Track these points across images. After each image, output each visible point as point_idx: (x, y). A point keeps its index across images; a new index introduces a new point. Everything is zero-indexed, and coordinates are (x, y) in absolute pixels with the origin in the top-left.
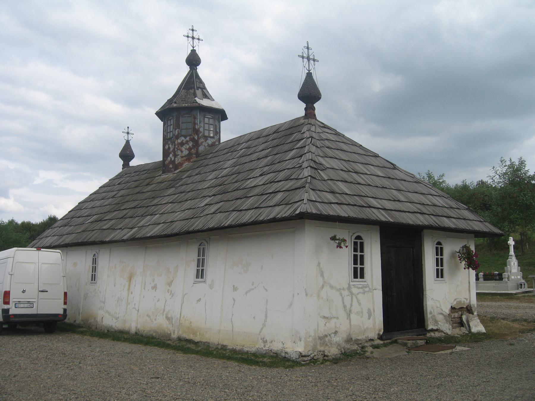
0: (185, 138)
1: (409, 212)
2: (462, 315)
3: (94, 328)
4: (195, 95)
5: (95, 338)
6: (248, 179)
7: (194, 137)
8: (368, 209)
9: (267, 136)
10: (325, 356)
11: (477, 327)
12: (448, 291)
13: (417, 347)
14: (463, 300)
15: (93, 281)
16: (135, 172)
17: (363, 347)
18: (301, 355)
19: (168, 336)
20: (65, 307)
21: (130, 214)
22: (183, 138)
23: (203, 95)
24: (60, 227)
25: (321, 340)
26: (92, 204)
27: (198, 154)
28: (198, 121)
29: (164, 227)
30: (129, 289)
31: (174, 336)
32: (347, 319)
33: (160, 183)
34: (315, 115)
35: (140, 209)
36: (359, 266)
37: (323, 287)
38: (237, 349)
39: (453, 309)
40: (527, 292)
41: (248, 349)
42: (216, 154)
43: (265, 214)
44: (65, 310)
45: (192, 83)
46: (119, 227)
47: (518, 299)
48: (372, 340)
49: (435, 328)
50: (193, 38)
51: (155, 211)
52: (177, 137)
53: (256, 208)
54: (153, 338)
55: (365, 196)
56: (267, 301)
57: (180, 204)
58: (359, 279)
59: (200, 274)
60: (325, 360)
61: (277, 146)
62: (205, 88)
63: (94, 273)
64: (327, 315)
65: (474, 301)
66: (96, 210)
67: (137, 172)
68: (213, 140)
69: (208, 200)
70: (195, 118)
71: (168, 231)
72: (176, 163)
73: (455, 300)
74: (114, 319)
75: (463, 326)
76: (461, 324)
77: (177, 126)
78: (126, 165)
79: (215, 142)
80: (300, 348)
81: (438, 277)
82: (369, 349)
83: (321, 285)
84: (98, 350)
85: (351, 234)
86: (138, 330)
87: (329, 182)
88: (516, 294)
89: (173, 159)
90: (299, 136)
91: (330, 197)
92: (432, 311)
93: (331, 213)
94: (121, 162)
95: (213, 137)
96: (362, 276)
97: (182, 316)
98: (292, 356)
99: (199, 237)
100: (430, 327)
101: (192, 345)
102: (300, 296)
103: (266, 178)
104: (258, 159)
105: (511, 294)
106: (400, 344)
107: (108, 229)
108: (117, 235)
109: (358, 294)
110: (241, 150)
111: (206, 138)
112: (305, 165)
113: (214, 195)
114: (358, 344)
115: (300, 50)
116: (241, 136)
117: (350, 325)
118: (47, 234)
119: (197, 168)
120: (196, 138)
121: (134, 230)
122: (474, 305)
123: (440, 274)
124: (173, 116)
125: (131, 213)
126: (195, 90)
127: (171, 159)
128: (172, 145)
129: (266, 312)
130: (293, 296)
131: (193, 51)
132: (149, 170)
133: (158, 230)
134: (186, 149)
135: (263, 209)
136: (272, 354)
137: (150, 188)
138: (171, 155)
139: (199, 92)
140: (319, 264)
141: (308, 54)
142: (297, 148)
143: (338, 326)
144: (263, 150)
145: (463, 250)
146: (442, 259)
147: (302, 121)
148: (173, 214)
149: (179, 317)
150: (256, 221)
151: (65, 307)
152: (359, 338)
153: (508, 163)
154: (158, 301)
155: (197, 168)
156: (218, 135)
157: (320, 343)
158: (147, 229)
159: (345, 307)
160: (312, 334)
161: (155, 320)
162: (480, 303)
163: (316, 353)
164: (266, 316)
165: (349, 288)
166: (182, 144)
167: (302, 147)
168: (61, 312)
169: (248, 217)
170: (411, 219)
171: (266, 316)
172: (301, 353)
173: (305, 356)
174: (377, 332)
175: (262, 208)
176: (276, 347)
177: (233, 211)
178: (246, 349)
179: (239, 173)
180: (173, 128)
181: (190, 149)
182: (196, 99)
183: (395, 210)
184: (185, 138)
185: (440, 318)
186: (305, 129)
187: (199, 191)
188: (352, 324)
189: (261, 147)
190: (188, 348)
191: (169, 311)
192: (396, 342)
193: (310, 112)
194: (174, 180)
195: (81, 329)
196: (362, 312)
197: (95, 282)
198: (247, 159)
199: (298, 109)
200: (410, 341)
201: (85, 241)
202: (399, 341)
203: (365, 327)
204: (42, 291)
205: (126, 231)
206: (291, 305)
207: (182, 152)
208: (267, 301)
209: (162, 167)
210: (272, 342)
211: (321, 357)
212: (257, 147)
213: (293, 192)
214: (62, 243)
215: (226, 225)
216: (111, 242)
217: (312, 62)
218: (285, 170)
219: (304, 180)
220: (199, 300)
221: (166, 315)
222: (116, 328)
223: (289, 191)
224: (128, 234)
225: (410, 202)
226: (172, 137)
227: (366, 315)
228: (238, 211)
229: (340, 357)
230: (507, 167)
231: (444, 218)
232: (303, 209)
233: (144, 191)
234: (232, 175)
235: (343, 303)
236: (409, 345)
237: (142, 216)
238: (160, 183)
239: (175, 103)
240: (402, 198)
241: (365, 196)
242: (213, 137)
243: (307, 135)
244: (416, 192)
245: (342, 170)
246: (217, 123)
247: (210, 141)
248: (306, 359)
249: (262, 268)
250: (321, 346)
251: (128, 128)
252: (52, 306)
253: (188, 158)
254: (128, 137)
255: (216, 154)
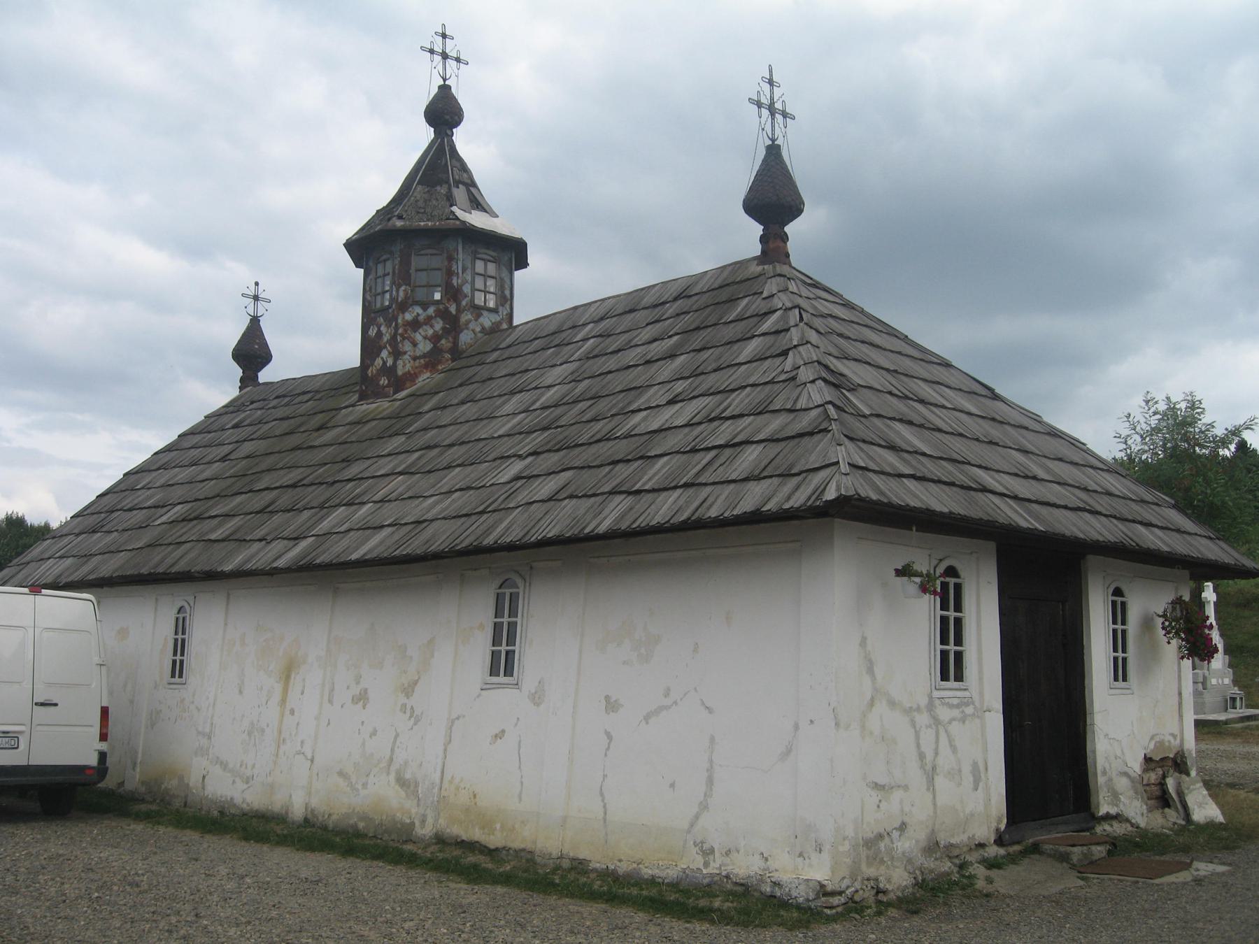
0: (425, 309)
1: (1066, 507)
2: (1164, 777)
3: (177, 804)
4: (451, 201)
5: (188, 832)
6: (633, 412)
7: (447, 309)
8: (980, 494)
9: (656, 306)
10: (878, 893)
11: (1205, 809)
12: (1138, 712)
13: (1092, 863)
14: (1168, 738)
15: (177, 680)
16: (277, 397)
17: (962, 866)
18: (823, 891)
19: (405, 833)
20: (103, 746)
21: (258, 501)
22: (418, 310)
23: (471, 201)
24: (78, 535)
25: (869, 848)
26: (164, 477)
27: (456, 353)
28: (458, 267)
29: (396, 537)
30: (283, 702)
31: (425, 831)
32: (928, 789)
33: (358, 423)
34: (788, 255)
35: (311, 489)
36: (952, 647)
37: (872, 703)
38: (620, 872)
39: (1148, 760)
40: (1249, 718)
41: (656, 872)
42: (507, 353)
43: (718, 505)
44: (103, 756)
45: (440, 171)
46: (259, 533)
47: (1235, 734)
48: (981, 846)
49: (1113, 811)
50: (445, 56)
51: (359, 496)
52: (403, 307)
53: (687, 485)
54: (358, 834)
55: (963, 463)
56: (712, 739)
57: (432, 478)
58: (952, 684)
59: (503, 664)
60: (880, 902)
61: (698, 328)
62: (474, 184)
63: (178, 658)
64: (882, 780)
65: (1190, 741)
66: (178, 493)
67: (284, 396)
68: (495, 318)
69: (516, 467)
70: (450, 259)
71: (415, 546)
72: (400, 373)
73: (1152, 738)
74: (238, 780)
75: (1168, 806)
76: (1163, 800)
77: (403, 277)
78: (249, 379)
79: (500, 323)
80: (820, 871)
81: (944, 677)
82: (980, 871)
83: (869, 697)
84: (223, 870)
85: (934, 562)
86: (312, 811)
87: (875, 420)
88: (1226, 722)
89: (390, 362)
90: (758, 305)
91: (890, 460)
92: (1107, 766)
93: (912, 504)
94: (238, 372)
95: (495, 311)
96: (959, 677)
97: (447, 777)
98: (794, 894)
99: (502, 566)
100: (1104, 809)
101: (482, 858)
102: (811, 723)
103: (688, 411)
104: (648, 362)
105: (1216, 723)
106: (1050, 856)
107: (223, 540)
108: (253, 556)
109: (950, 722)
110: (585, 340)
111: (478, 310)
112: (805, 374)
113: (535, 453)
114: (950, 858)
115: (753, 85)
116: (576, 308)
117: (935, 804)
118: (42, 553)
119: (460, 385)
120: (453, 309)
121: (304, 544)
122: (1190, 752)
123: (1120, 671)
124: (392, 253)
125: (286, 499)
126: (450, 189)
127: (384, 363)
128: (389, 326)
129: (710, 770)
130: (796, 727)
131: (445, 90)
132: (317, 392)
133: (382, 542)
134: (425, 338)
135: (708, 489)
136: (729, 886)
137: (329, 436)
138: (384, 354)
139: (460, 193)
140: (864, 639)
141: (772, 98)
142: (763, 334)
143: (907, 809)
144: (655, 340)
145: (1174, 609)
146: (1124, 632)
147: (756, 269)
148: (417, 502)
149: (438, 781)
150: (699, 520)
151: (103, 746)
152: (953, 841)
153: (1162, 407)
154: (374, 733)
155: (460, 385)
156: (507, 306)
157: (868, 857)
158: (345, 542)
159: (922, 756)
160: (850, 832)
161: (365, 785)
162: (1203, 746)
163: (857, 885)
164: (710, 782)
165: (931, 707)
166: (415, 324)
167: (777, 332)
168: (93, 761)
169: (664, 509)
170: (1075, 525)
171: (710, 782)
172: (822, 886)
173: (833, 894)
174: (994, 825)
175: (705, 484)
176: (744, 866)
177: (613, 492)
178: (647, 872)
179: (597, 397)
180: (393, 283)
181: (435, 339)
182: (454, 209)
183: (1036, 502)
184: (425, 309)
185: (1122, 784)
186: (771, 287)
187: (481, 444)
188: (939, 804)
189: (646, 334)
190: (475, 867)
191: (406, 763)
192: (1035, 849)
193: (774, 246)
194: (396, 416)
195: (143, 807)
196: (960, 771)
197: (183, 680)
198: (612, 363)
199: (746, 239)
200: (1075, 849)
201: (160, 570)
202: (1047, 847)
203: (967, 811)
204: (42, 704)
205: (278, 546)
206: (789, 751)
207: (415, 344)
208: (712, 739)
209: (359, 383)
210: (728, 853)
211: (869, 895)
212: (635, 333)
213: (792, 443)
214: (91, 577)
215: (602, 529)
216: (240, 575)
217: (779, 117)
218: (745, 387)
219: (814, 413)
220: (500, 735)
221: (398, 772)
222: (245, 806)
223: (778, 440)
224: (293, 554)
225: (1059, 483)
226: (389, 307)
227: (968, 780)
228: (629, 493)
229: (913, 894)
230: (1158, 417)
231: (1139, 526)
232: (847, 488)
233: (316, 443)
234: (576, 402)
235: (918, 746)
236: (1075, 859)
237: (322, 507)
238: (358, 423)
239: (400, 217)
240: (1041, 474)
241: (963, 463)
242: (495, 311)
243: (781, 301)
244: (1060, 460)
245: (890, 393)
246: (505, 274)
247: (487, 320)
248: (835, 901)
249: (696, 650)
250: (869, 864)
251: (257, 284)
252: (68, 744)
253: (431, 361)
254: (256, 308)
255: (507, 353)
